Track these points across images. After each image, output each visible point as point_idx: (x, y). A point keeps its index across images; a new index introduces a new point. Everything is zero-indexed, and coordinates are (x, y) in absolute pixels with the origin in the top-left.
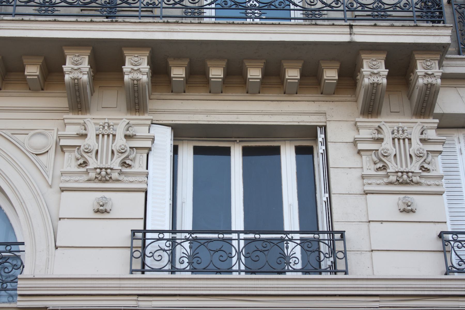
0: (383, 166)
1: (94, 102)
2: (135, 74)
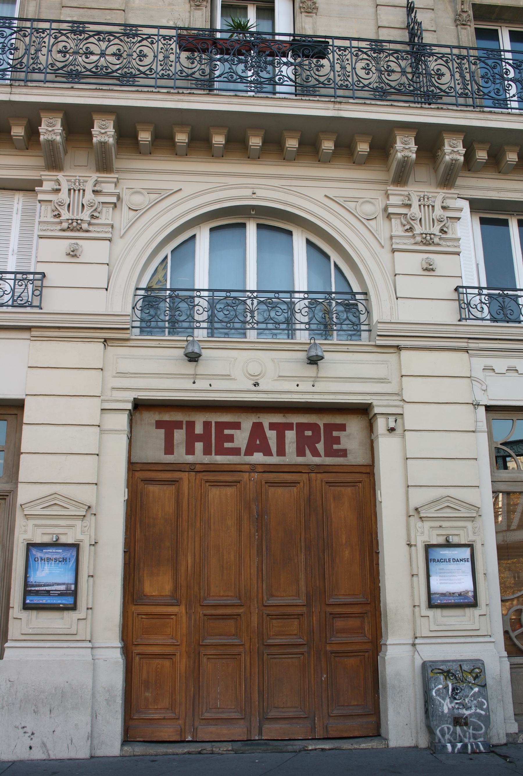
0: (58, 214)
1: (67, 161)
2: (455, 155)
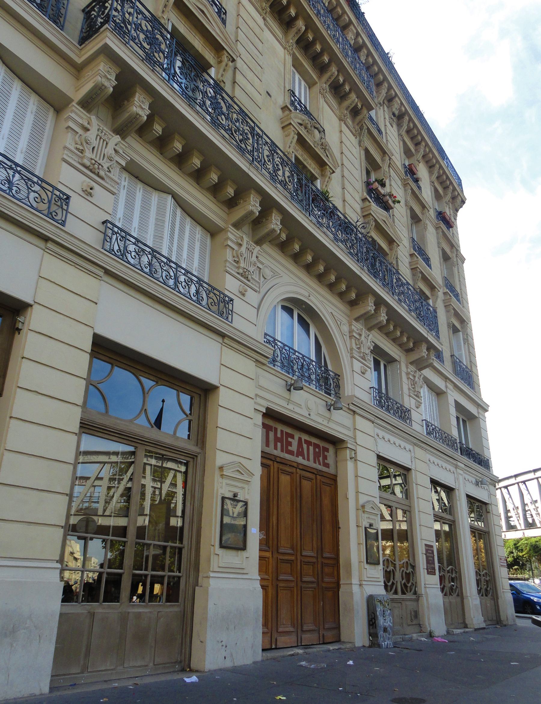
0: (82, 150)
